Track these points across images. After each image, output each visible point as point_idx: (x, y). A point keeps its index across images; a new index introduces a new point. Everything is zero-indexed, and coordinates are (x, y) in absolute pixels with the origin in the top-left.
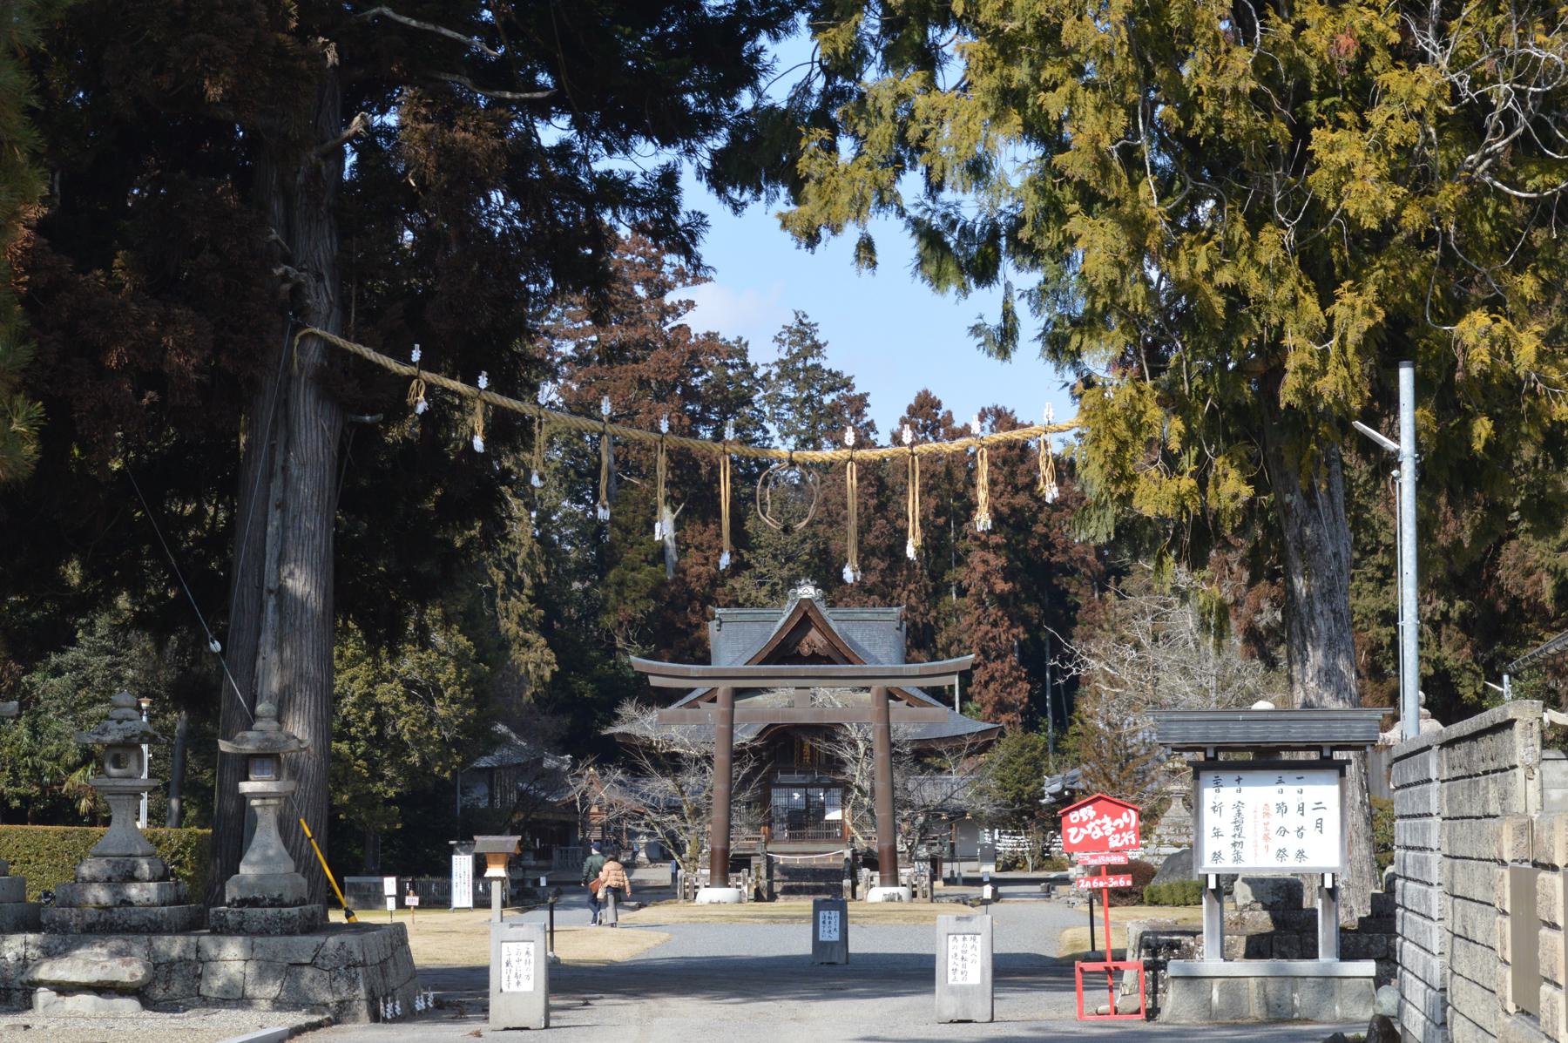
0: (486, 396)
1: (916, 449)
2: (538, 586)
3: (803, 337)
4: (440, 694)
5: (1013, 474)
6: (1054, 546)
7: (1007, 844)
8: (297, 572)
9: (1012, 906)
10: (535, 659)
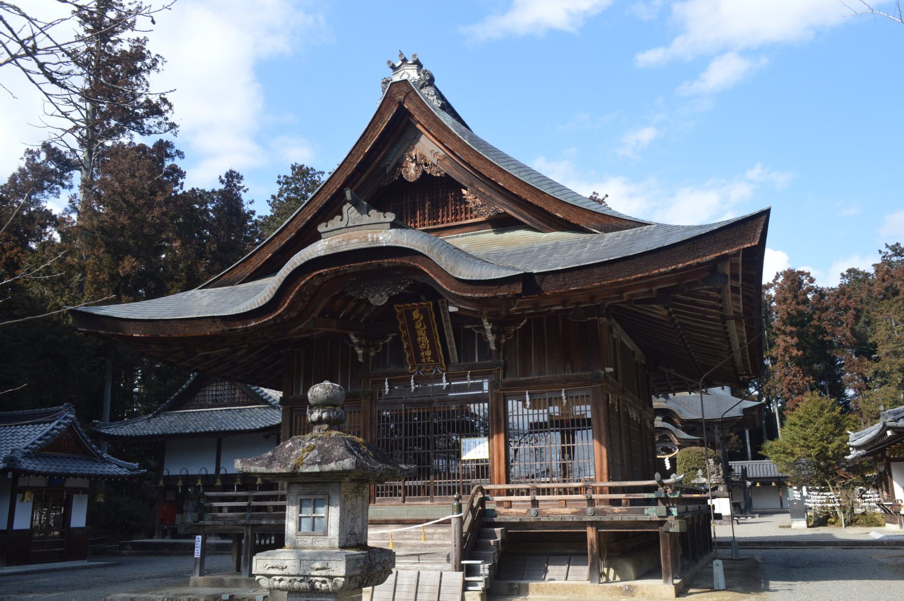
5: (796, 297)
6: (826, 332)
7: (815, 500)
9: (571, 186)
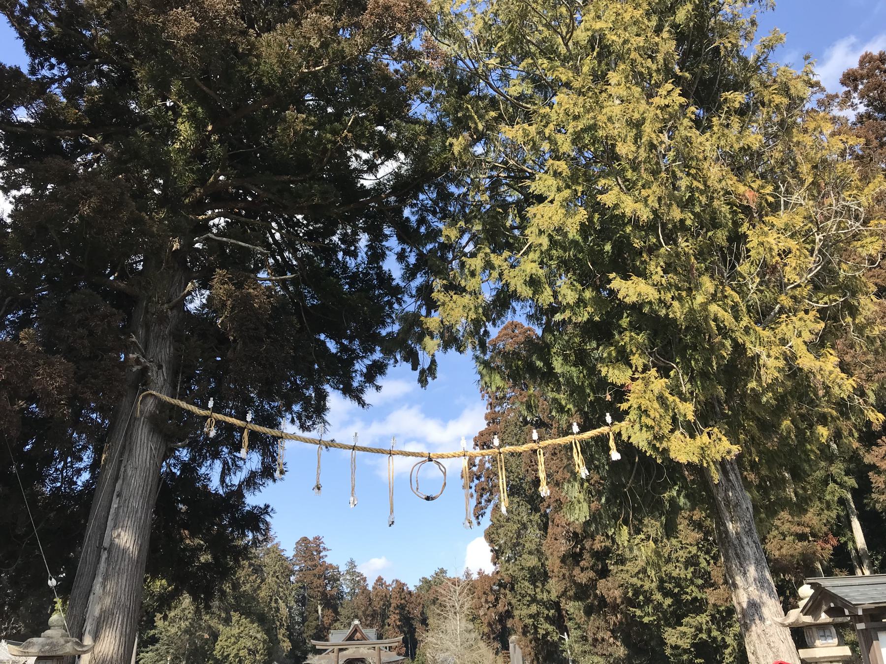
0: (250, 426)
1: (501, 450)
2: (288, 626)
3: (352, 564)
4: (258, 652)
8: (122, 534)
10: (286, 645)
